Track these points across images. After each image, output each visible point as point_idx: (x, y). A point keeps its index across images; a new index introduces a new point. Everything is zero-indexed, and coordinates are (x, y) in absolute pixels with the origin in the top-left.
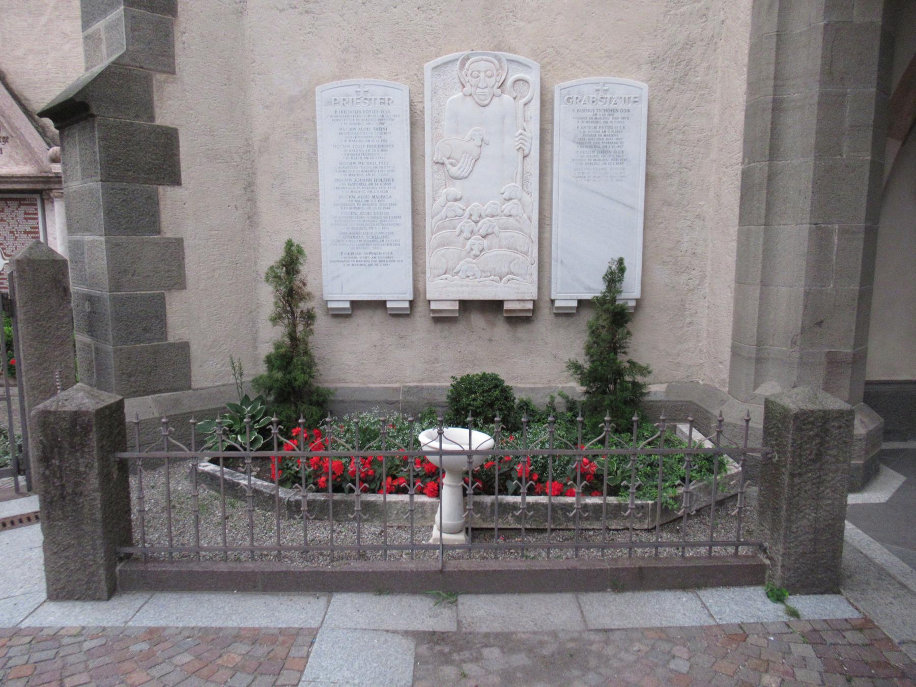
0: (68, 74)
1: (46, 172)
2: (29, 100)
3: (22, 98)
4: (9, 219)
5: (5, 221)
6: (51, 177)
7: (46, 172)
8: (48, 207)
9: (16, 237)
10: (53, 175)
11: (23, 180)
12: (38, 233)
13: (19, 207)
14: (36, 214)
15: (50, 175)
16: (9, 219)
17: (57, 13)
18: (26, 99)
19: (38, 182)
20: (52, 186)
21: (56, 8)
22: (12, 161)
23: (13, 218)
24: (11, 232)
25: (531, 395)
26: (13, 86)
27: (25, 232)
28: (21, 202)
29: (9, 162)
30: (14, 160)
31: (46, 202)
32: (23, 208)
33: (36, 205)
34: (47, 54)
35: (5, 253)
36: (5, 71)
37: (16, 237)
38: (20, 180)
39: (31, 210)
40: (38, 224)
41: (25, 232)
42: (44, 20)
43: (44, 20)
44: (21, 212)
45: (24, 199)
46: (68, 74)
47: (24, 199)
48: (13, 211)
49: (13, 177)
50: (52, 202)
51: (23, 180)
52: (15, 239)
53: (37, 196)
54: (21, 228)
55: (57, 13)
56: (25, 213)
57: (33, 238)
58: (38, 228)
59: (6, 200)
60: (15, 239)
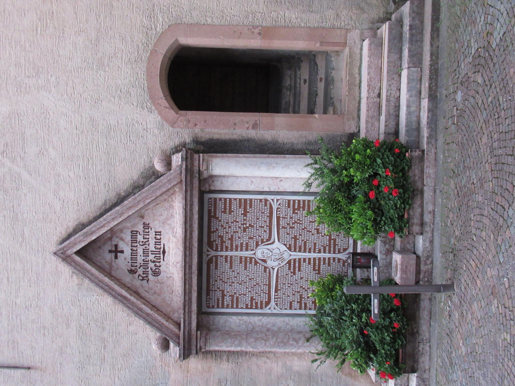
0: (80, 154)
1: (181, 173)
2: (106, 201)
3: (103, 208)
4: (231, 231)
5: (232, 236)
6: (186, 166)
7: (181, 173)
8: (218, 185)
9: (250, 225)
10: (184, 163)
11: (189, 198)
12: (245, 200)
13: (218, 218)
14: (225, 199)
15: (184, 166)
16: (231, 231)
17: (19, 160)
18: (105, 204)
19: (192, 183)
20: (196, 169)
21: (13, 160)
22: (169, 222)
23: (230, 227)
24: (245, 231)
25: (79, 220)
26: (92, 216)
27: (245, 214)
28: (212, 216)
29: (170, 225)
30: (168, 219)
31: (213, 188)
32: (219, 214)
33: (215, 199)
34: (59, 176)
35: (267, 240)
36: (76, 223)
37: (250, 225)
38: (188, 203)
39: (220, 205)
40: (235, 199)
41: (245, 214)
42: (25, 175)
43: (25, 175)
44: (224, 217)
45: (209, 211)
46: (80, 154)
47: (209, 211)
48: (222, 226)
49: (186, 223)
50: (212, 177)
51: (189, 198)
52: (253, 226)
53: (207, 196)
54: (240, 219)
55: (19, 160)
56: (225, 212)
57: (251, 207)
58: (240, 200)
59: (210, 232)
60: (253, 226)
